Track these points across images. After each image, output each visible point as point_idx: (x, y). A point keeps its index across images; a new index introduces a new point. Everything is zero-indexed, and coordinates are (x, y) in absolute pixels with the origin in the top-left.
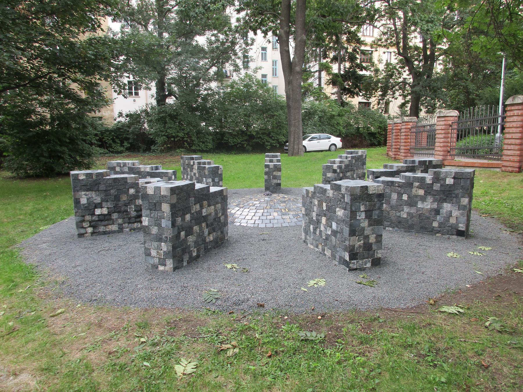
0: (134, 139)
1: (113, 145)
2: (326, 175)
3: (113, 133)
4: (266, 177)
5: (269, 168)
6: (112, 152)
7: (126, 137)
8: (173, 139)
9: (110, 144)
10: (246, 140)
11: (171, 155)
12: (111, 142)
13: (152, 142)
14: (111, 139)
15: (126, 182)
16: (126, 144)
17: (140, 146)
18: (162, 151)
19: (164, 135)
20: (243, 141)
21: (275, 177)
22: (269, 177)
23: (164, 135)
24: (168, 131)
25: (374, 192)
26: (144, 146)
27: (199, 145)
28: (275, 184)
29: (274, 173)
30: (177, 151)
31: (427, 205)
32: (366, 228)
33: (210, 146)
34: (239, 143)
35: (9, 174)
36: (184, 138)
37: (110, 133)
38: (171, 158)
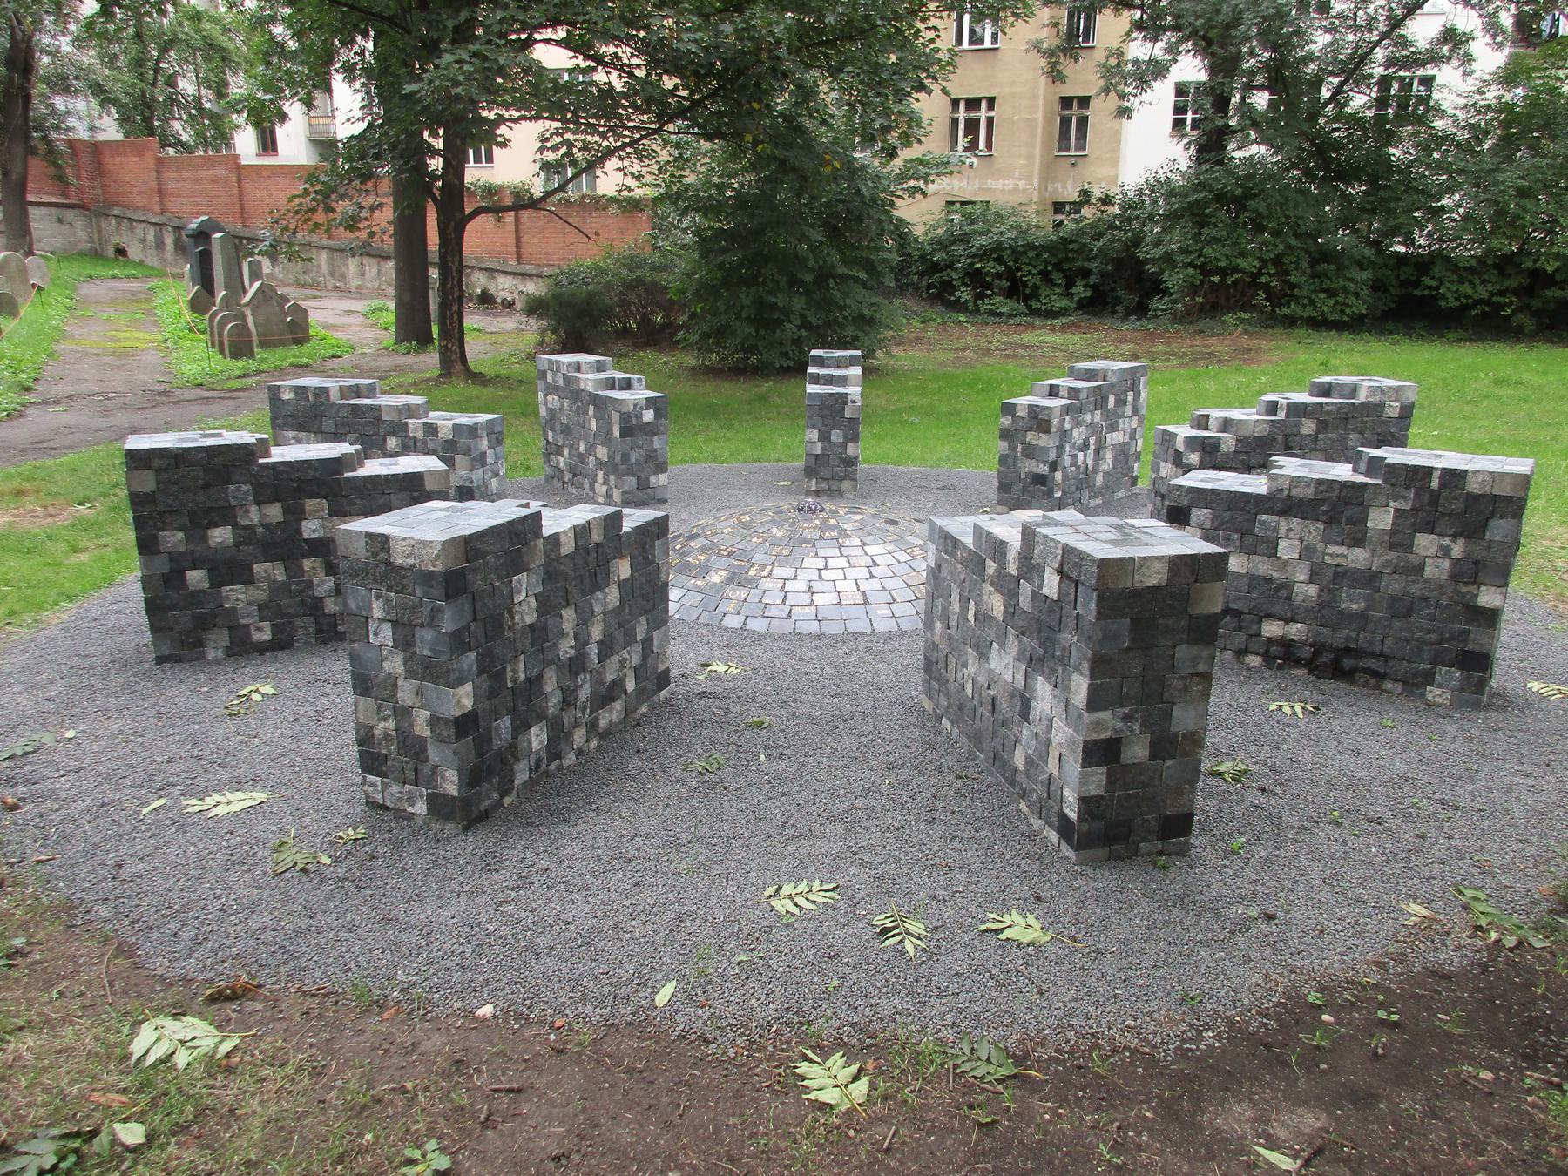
0: (1103, 275)
1: (1044, 290)
3: (1045, 255)
4: (1002, 446)
5: (1013, 416)
6: (1035, 313)
8: (1216, 279)
9: (1036, 287)
10: (1515, 292)
11: (1201, 332)
12: (1037, 280)
14: (1040, 273)
15: (379, 419)
16: (1080, 289)
18: (1177, 318)
19: (1191, 264)
20: (1502, 293)
21: (1031, 452)
22: (1013, 448)
23: (1191, 264)
24: (1208, 250)
25: (410, 561)
26: (1132, 299)
27: (1312, 302)
30: (1227, 318)
32: (400, 682)
33: (1358, 307)
34: (1481, 302)
35: (689, 359)
36: (1259, 274)
37: (1038, 255)
38: (1200, 345)
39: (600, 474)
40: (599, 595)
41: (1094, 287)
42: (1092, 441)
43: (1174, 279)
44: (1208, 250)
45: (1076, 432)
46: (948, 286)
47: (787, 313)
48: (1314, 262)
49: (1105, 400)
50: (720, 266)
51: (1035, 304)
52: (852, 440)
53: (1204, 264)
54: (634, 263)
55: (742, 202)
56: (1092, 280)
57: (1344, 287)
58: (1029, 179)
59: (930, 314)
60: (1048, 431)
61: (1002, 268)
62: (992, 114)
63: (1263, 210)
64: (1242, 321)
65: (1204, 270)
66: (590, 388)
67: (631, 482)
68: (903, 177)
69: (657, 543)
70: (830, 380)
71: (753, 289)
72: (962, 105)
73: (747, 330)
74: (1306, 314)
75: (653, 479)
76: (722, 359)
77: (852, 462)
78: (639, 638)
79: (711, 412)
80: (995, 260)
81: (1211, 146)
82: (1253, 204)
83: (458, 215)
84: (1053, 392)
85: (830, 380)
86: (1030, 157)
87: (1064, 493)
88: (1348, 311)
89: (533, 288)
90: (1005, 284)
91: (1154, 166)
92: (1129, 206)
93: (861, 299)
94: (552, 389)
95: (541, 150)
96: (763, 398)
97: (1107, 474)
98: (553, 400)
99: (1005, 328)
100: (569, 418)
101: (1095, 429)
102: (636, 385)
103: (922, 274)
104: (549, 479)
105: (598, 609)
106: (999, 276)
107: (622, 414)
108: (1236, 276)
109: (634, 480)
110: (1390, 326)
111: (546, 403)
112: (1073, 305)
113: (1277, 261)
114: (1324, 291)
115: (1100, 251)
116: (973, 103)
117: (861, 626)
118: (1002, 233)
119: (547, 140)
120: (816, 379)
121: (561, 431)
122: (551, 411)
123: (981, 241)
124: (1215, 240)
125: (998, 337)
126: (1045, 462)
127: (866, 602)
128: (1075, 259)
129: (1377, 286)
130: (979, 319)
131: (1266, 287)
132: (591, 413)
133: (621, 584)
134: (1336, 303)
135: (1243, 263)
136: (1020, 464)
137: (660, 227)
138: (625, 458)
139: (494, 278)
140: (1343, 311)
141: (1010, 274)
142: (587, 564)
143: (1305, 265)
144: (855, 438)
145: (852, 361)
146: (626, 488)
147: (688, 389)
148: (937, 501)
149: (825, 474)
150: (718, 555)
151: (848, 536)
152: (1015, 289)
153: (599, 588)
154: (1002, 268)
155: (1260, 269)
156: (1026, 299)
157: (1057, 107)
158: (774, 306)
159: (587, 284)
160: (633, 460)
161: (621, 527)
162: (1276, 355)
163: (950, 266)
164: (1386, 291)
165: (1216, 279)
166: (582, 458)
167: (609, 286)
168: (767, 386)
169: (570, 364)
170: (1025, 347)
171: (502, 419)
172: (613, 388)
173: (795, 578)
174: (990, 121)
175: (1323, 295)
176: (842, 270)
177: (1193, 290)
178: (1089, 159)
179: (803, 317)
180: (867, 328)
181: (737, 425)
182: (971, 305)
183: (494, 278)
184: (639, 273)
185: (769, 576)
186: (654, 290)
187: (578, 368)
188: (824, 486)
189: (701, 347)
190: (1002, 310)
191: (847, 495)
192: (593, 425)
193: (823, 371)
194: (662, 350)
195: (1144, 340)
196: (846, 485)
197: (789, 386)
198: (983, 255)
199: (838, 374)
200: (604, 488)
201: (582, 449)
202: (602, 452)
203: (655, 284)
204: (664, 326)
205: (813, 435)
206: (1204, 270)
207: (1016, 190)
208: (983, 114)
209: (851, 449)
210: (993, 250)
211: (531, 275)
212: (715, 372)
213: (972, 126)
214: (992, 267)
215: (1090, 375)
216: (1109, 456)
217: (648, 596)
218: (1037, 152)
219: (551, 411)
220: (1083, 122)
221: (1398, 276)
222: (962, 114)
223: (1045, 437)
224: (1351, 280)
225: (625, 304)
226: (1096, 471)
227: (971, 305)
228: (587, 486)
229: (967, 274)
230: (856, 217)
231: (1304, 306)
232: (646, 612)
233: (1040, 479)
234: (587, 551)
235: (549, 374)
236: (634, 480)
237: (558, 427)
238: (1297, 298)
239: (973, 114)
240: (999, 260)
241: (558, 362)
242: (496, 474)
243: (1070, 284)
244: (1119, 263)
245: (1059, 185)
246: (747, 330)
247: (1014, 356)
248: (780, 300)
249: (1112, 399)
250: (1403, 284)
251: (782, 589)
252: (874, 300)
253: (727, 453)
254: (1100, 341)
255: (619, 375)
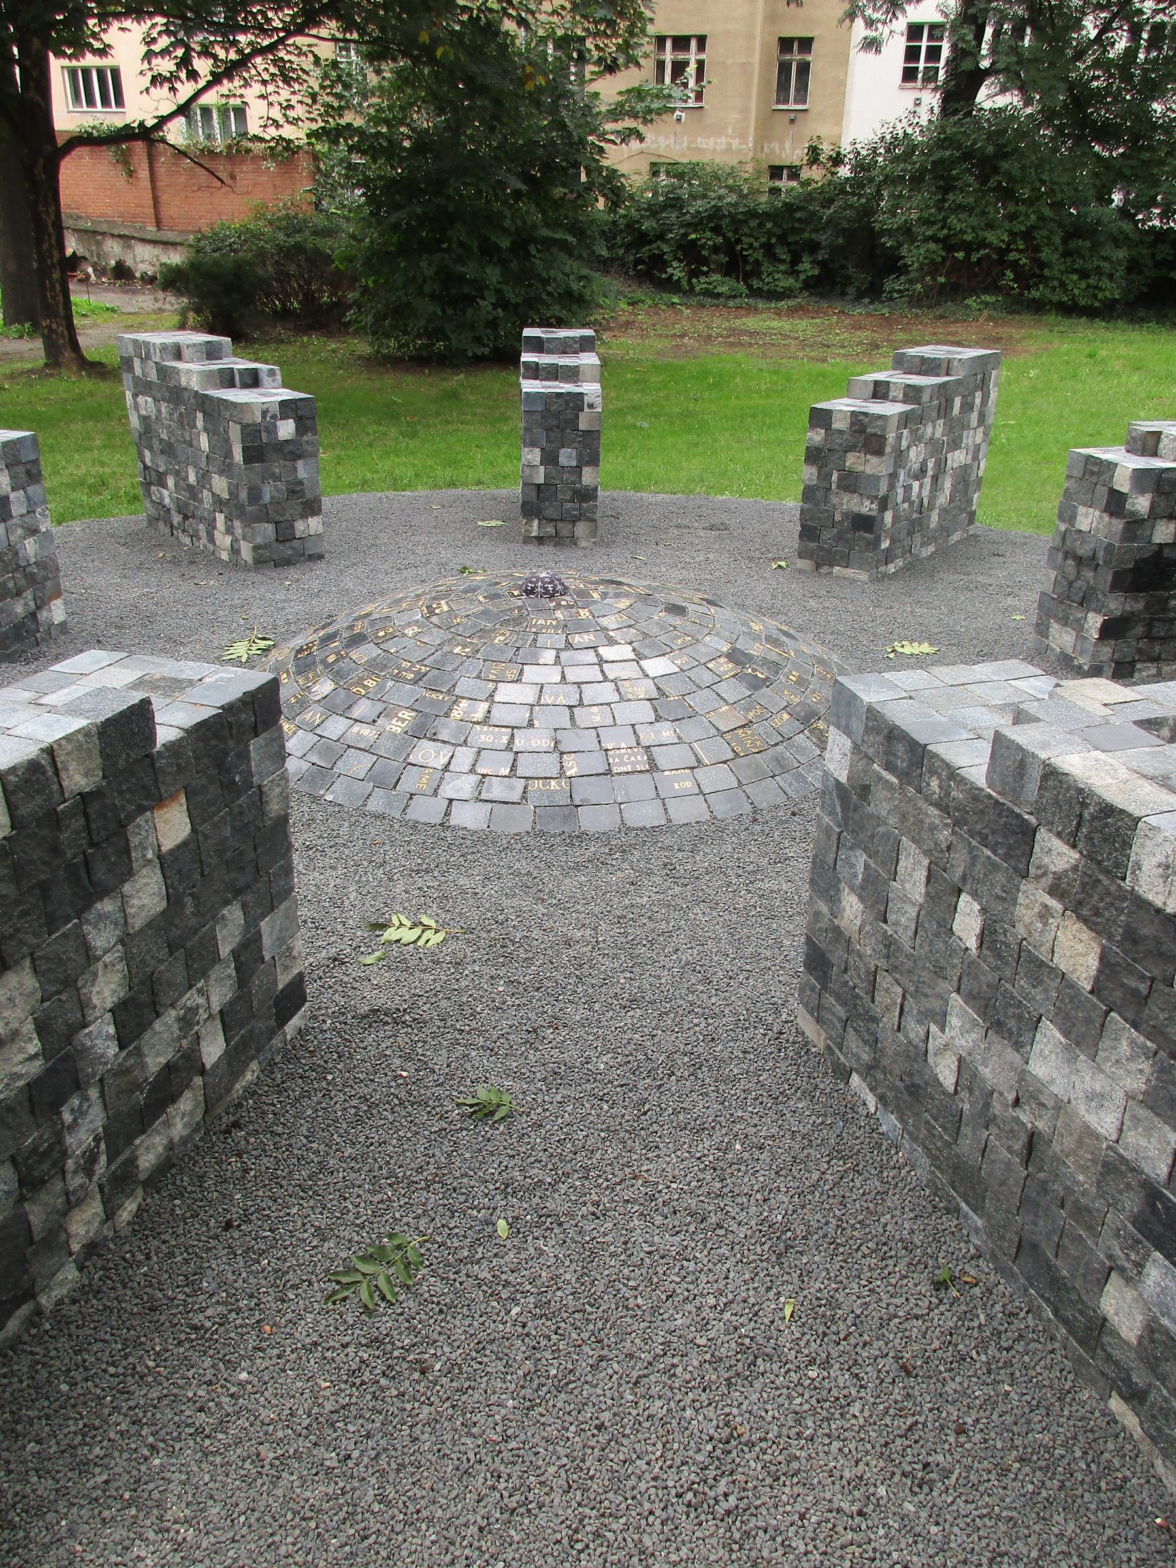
1: (767, 267)
2: (1072, 519)
3: (769, 225)
4: (809, 473)
5: (828, 429)
6: (755, 293)
7: (812, 240)
11: (942, 317)
12: (759, 255)
13: (892, 265)
14: (762, 246)
16: (806, 267)
17: (848, 277)
18: (916, 301)
19: (934, 239)
21: (851, 483)
22: (824, 477)
23: (934, 239)
24: (952, 220)
26: (863, 278)
27: (1063, 284)
28: (846, 515)
29: (852, 460)
30: (969, 302)
31: (1096, 1099)
33: (1111, 290)
35: (363, 347)
36: (1008, 250)
37: (761, 225)
39: (220, 518)
40: (107, 906)
41: (823, 264)
42: (930, 464)
43: (914, 255)
44: (952, 220)
45: (913, 453)
46: (659, 262)
47: (480, 287)
48: (1068, 237)
49: (949, 403)
50: (395, 227)
51: (756, 283)
52: (589, 464)
53: (947, 237)
54: (292, 225)
55: (422, 142)
56: (821, 255)
57: (1098, 267)
58: (743, 136)
59: (639, 294)
60: (879, 452)
61: (720, 240)
62: (703, 57)
63: (1016, 172)
64: (987, 304)
65: (948, 244)
66: (195, 384)
67: (267, 530)
68: (616, 113)
69: (255, 745)
70: (554, 373)
71: (437, 257)
72: (669, 44)
73: (431, 309)
74: (1055, 298)
75: (300, 526)
76: (401, 346)
77: (588, 495)
78: (225, 951)
79: (390, 414)
80: (712, 230)
81: (960, 89)
82: (1005, 165)
83: (49, 148)
84: (880, 391)
85: (554, 373)
86: (745, 110)
87: (893, 541)
88: (1100, 296)
89: (175, 258)
90: (723, 258)
91: (892, 119)
92: (861, 166)
93: (568, 270)
94: (143, 387)
95: (149, 56)
96: (454, 395)
97: (944, 511)
98: (146, 403)
99: (724, 311)
100: (171, 433)
101: (936, 448)
102: (265, 379)
103: (628, 247)
104: (153, 521)
105: (102, 938)
106: (716, 249)
107: (245, 427)
108: (982, 252)
109: (269, 528)
110: (1141, 313)
111: (136, 407)
112: (799, 285)
113: (1027, 235)
114: (1075, 271)
115: (829, 222)
116: (681, 43)
117: (645, 814)
118: (720, 198)
119: (154, 40)
120: (535, 372)
121: (161, 450)
122: (144, 419)
123: (699, 205)
124: (961, 208)
125: (718, 322)
126: (872, 499)
127: (653, 767)
128: (802, 230)
129: (1133, 267)
130: (693, 301)
131: (1014, 265)
132: (200, 423)
133: (166, 862)
134: (1088, 286)
135: (991, 237)
136: (834, 500)
137: (324, 185)
138: (255, 495)
139: (130, 247)
140: (1095, 296)
141: (729, 248)
142: (56, 850)
143: (1057, 240)
144: (594, 461)
145: (585, 345)
146: (259, 541)
147: (361, 384)
148: (709, 549)
149: (550, 512)
150: (398, 678)
151: (612, 642)
152: (735, 266)
153: (104, 892)
154: (720, 240)
155: (1008, 245)
156: (747, 277)
157: (775, 49)
158: (461, 278)
159: (235, 251)
160: (267, 498)
161: (151, 737)
162: (1032, 345)
163: (661, 237)
164: (1140, 272)
165: (960, 255)
166: (193, 493)
167: (262, 254)
168: (457, 380)
169: (164, 348)
170: (751, 334)
171: (34, 439)
172: (232, 385)
173: (531, 724)
174: (701, 65)
175: (1075, 277)
176: (546, 232)
177: (933, 268)
178: (810, 115)
179: (498, 292)
180: (575, 307)
181: (422, 433)
182: (684, 283)
183: (130, 247)
184: (298, 238)
185: (486, 721)
186: (318, 259)
187: (178, 353)
188: (550, 529)
189: (377, 332)
190: (720, 290)
191: (583, 544)
192: (204, 442)
193: (545, 359)
194: (330, 335)
195: (881, 326)
196: (581, 529)
197: (490, 380)
198: (698, 224)
199: (569, 364)
200: (228, 540)
201: (192, 479)
202: (220, 484)
203: (318, 252)
204: (334, 305)
205: (533, 456)
206: (948, 244)
207: (728, 150)
208: (692, 56)
209: (588, 476)
210: (710, 218)
211: (174, 244)
212: (394, 362)
213: (679, 68)
214: (708, 239)
215: (927, 366)
216: (948, 484)
217: (246, 849)
218: (753, 105)
219: (144, 419)
220: (804, 68)
221: (1153, 255)
222: (668, 56)
223: (874, 460)
224: (1106, 259)
225: (283, 277)
226: (931, 507)
227: (684, 283)
228: (203, 534)
229: (680, 247)
230: (559, 161)
231: (1054, 289)
232: (238, 892)
233: (864, 523)
234: (54, 820)
235: (137, 363)
236: (269, 528)
237: (156, 445)
238: (1047, 279)
239: (681, 56)
240: (717, 230)
241: (147, 344)
242: (33, 531)
243: (796, 260)
244: (849, 234)
245: (776, 146)
246: (431, 309)
247: (740, 344)
248: (469, 271)
249: (958, 402)
250: (1158, 265)
251: (509, 748)
252: (585, 272)
253: (410, 473)
254: (831, 326)
255: (242, 364)
